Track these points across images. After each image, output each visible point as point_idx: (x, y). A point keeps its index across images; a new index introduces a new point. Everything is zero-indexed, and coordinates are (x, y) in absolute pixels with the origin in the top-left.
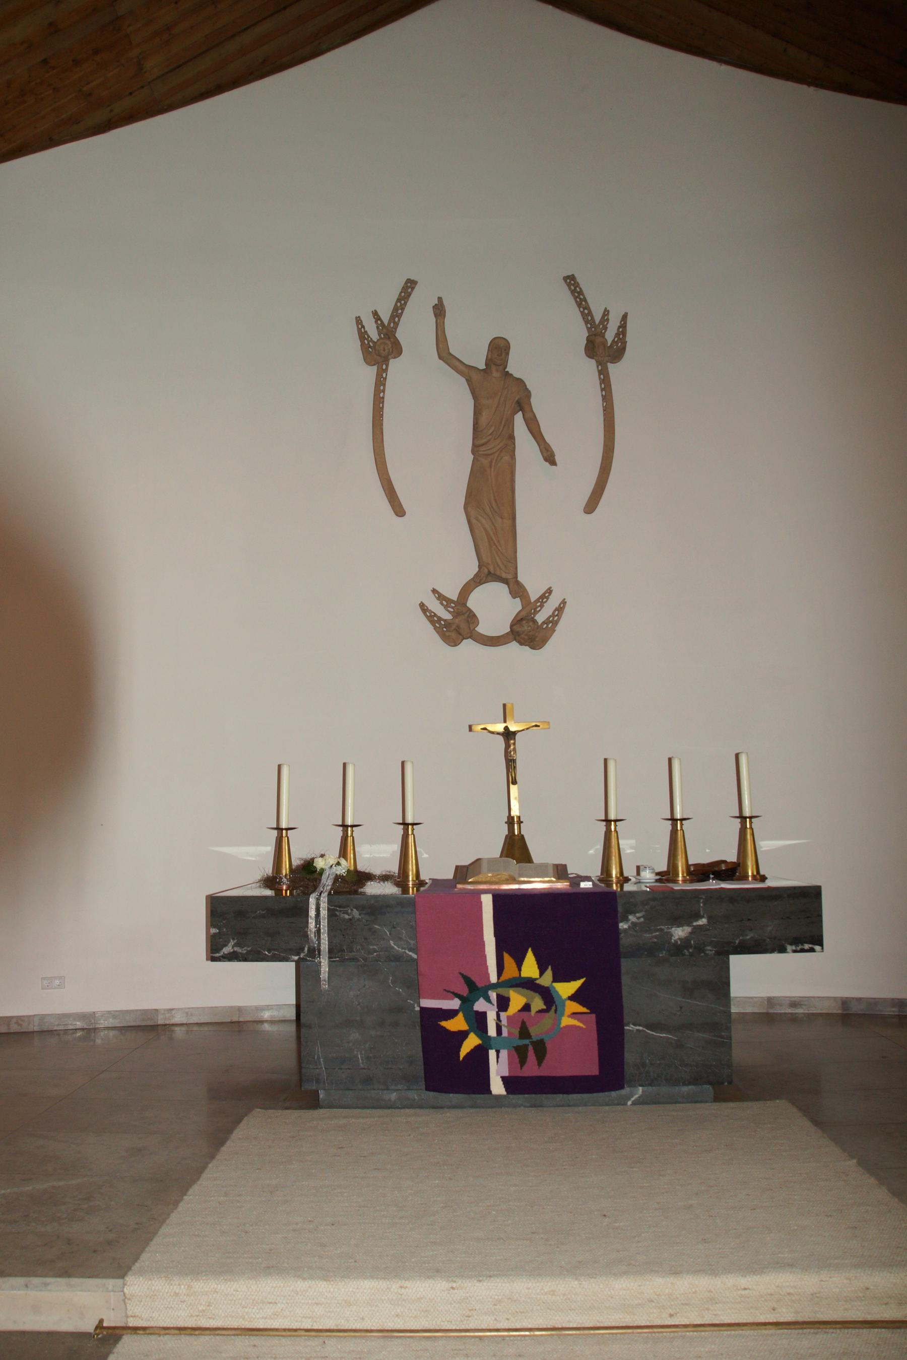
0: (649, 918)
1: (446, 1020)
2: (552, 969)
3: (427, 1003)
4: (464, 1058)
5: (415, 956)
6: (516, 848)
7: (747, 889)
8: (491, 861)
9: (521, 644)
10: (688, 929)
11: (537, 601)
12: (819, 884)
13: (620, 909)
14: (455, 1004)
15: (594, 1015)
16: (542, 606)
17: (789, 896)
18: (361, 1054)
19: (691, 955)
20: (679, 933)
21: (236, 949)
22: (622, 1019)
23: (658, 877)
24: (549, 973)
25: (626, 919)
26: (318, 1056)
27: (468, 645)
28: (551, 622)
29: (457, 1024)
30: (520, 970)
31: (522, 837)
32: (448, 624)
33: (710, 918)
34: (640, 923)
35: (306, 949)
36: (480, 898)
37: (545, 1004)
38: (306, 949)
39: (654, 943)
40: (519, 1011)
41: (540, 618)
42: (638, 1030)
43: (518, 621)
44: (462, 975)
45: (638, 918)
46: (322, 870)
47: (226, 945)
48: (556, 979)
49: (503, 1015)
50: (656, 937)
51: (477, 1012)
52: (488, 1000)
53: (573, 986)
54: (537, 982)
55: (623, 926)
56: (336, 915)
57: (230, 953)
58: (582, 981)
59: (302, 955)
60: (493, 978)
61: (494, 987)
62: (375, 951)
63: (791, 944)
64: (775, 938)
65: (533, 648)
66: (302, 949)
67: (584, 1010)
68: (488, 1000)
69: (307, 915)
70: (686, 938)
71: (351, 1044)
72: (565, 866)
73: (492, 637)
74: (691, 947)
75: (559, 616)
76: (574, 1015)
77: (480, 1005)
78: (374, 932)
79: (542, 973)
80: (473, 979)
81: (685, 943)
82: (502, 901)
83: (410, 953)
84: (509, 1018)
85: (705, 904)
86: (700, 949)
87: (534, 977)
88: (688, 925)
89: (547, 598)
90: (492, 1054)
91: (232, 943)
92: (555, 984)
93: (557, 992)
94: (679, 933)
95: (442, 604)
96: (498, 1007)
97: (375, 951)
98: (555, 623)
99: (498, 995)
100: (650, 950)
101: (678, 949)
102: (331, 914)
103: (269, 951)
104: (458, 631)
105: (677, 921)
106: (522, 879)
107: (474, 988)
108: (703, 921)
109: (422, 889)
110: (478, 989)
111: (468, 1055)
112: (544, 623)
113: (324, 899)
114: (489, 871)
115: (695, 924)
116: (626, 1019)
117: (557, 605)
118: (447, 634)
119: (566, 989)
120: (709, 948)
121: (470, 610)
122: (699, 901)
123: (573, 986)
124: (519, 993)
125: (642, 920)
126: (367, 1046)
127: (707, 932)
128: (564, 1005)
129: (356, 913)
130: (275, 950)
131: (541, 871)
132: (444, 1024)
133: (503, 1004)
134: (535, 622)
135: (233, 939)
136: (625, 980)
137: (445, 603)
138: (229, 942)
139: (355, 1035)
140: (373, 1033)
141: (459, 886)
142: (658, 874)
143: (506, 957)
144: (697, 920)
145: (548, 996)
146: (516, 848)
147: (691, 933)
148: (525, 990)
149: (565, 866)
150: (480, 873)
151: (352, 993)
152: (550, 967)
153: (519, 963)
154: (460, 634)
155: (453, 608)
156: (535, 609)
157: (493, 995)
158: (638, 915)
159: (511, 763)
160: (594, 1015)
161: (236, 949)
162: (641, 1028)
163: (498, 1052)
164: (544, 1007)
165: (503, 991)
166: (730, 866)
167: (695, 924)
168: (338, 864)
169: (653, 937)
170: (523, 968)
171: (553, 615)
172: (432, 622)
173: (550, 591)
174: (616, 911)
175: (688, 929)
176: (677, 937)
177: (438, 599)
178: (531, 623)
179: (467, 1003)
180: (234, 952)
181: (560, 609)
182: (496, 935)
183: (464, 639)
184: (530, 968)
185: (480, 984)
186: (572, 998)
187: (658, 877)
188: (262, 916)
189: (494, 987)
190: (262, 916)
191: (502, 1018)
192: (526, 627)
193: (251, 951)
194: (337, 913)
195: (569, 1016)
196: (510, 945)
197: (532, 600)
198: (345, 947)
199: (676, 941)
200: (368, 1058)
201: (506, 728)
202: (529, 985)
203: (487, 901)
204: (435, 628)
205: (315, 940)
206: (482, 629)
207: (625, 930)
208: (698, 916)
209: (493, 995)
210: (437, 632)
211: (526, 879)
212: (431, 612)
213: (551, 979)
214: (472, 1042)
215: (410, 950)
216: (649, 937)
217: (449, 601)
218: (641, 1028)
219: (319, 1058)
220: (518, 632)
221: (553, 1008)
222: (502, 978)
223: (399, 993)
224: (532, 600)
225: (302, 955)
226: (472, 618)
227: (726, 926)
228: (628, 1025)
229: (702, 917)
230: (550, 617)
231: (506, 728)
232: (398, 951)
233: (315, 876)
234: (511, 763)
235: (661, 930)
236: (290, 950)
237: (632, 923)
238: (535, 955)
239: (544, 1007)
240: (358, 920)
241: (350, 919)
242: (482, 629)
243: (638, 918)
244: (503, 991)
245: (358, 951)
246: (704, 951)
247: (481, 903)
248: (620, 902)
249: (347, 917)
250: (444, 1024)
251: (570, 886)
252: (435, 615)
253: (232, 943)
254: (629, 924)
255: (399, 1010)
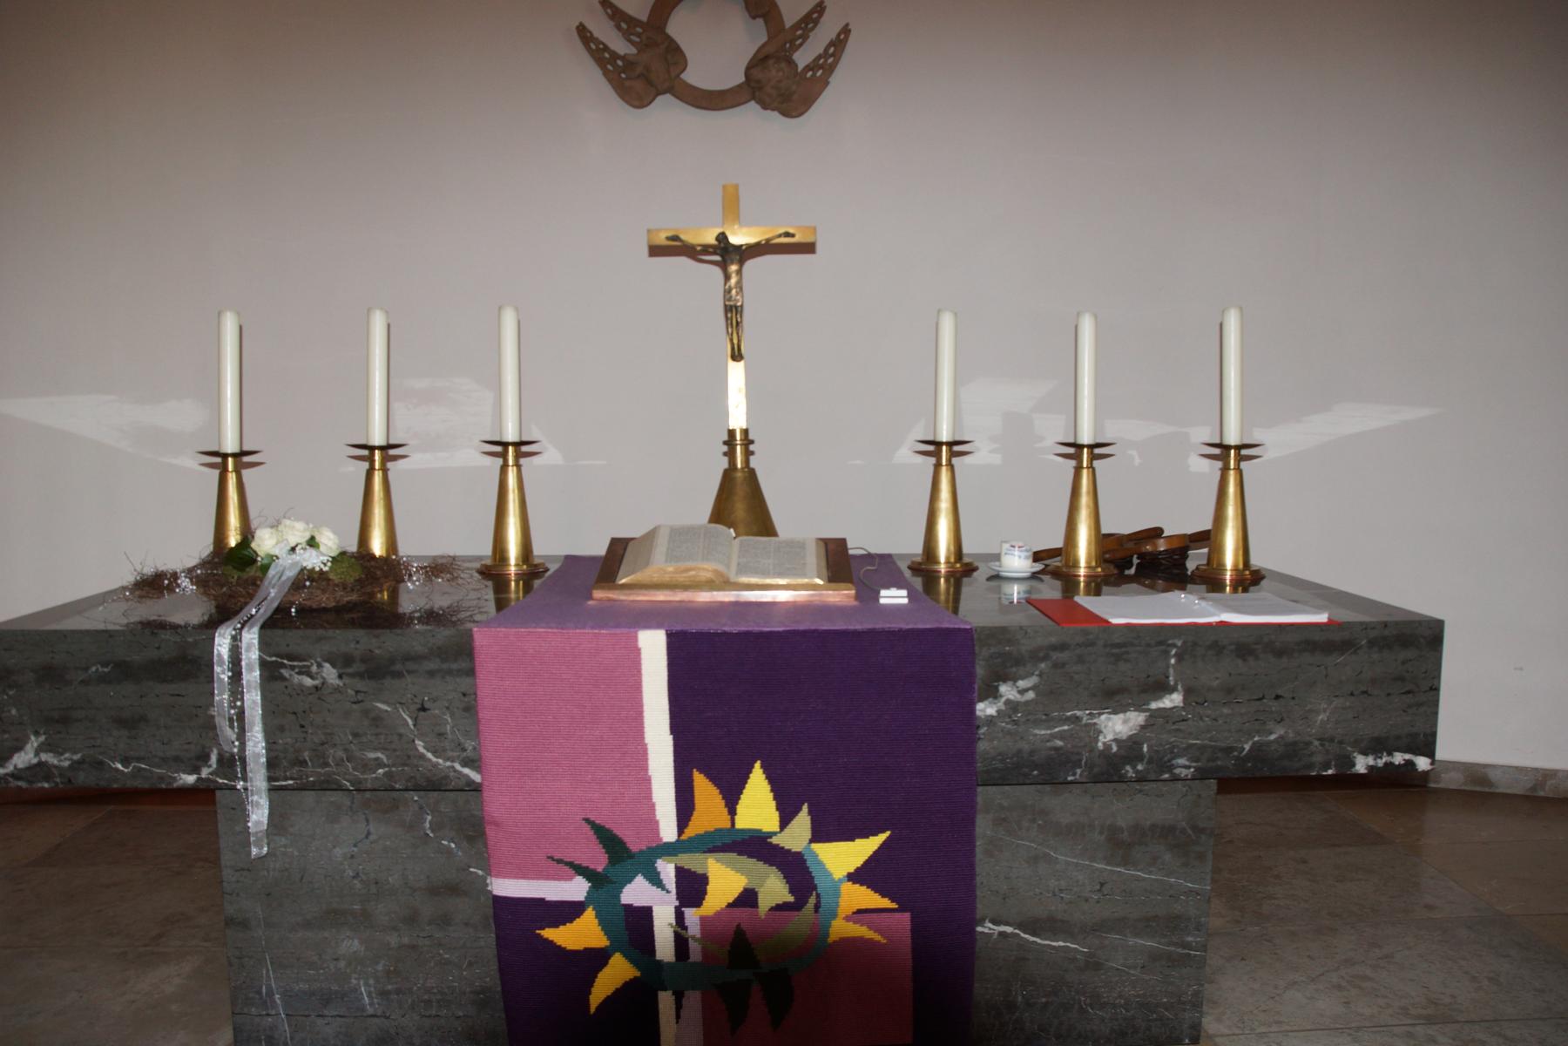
0: (1049, 693)
1: (556, 925)
2: (810, 813)
3: (507, 887)
4: (598, 1009)
5: (476, 777)
6: (741, 503)
7: (1280, 626)
8: (681, 534)
9: (765, 107)
10: (1136, 719)
11: (796, 26)
12: (1406, 592)
13: (980, 671)
14: (575, 889)
15: (907, 915)
16: (805, 37)
17: (1372, 643)
18: (366, 984)
19: (1141, 779)
20: (1117, 726)
21: (44, 757)
22: (974, 909)
23: (1039, 567)
24: (803, 821)
25: (992, 693)
26: (269, 988)
27: (666, 110)
28: (821, 67)
29: (583, 933)
30: (732, 812)
31: (751, 475)
32: (629, 63)
33: (1188, 693)
34: (1027, 703)
35: (214, 758)
36: (636, 639)
37: (791, 891)
38: (214, 758)
39: (1056, 749)
40: (730, 905)
41: (803, 58)
42: (1001, 934)
43: (758, 62)
44: (587, 820)
45: (1022, 692)
46: (272, 558)
47: (19, 749)
48: (819, 835)
49: (691, 915)
50: (1061, 736)
51: (629, 907)
52: (656, 880)
53: (862, 849)
54: (774, 840)
55: (985, 709)
56: (283, 679)
57: (31, 768)
58: (882, 837)
59: (205, 773)
60: (668, 832)
61: (668, 850)
62: (380, 764)
63: (1365, 753)
64: (1332, 740)
65: (786, 114)
66: (205, 758)
67: (886, 903)
68: (656, 880)
69: (210, 678)
70: (1130, 737)
71: (342, 964)
72: (843, 541)
73: (711, 93)
74: (1140, 758)
75: (837, 56)
76: (861, 914)
77: (636, 892)
78: (377, 720)
79: (785, 822)
80: (618, 832)
81: (1130, 748)
82: (694, 655)
83: (466, 771)
84: (703, 919)
85: (1179, 657)
86: (1161, 763)
87: (766, 829)
88: (1139, 709)
89: (816, 22)
90: (666, 1000)
91: (34, 742)
92: (816, 847)
93: (820, 864)
94: (1117, 726)
95: (619, 28)
96: (679, 896)
97: (380, 764)
98: (830, 69)
99: (680, 871)
100: (1049, 771)
101: (1111, 769)
102: (270, 672)
103: (126, 761)
104: (646, 77)
105: (1114, 698)
106: (745, 580)
107: (622, 855)
108: (1174, 700)
109: (537, 583)
110: (631, 855)
111: (608, 1001)
112: (808, 68)
113: (251, 637)
114: (670, 557)
115: (1154, 705)
116: (981, 909)
117: (833, 36)
118: (627, 83)
119: (841, 858)
120: (1182, 761)
121: (669, 37)
122: (1166, 653)
123: (862, 849)
124: (728, 864)
125: (1031, 695)
126: (380, 967)
127: (1182, 726)
128: (837, 894)
129: (330, 673)
130: (139, 760)
131: (789, 564)
132: (549, 933)
133: (691, 888)
134: (791, 63)
135: (37, 734)
136: (983, 826)
137: (624, 26)
138: (25, 741)
139: (351, 945)
140: (393, 940)
141: (598, 594)
142: (1037, 557)
143: (700, 782)
144: (1160, 698)
145: (796, 869)
146: (741, 503)
147: (1143, 727)
148: (744, 858)
149: (843, 541)
150: (647, 564)
151: (338, 852)
152: (805, 808)
153: (732, 796)
154: (650, 83)
155: (639, 35)
156: (792, 42)
157: (667, 869)
158: (1022, 684)
159: (559, 861)
160: (907, 915)
161: (44, 757)
162: (1009, 929)
163: (679, 997)
164: (791, 899)
165: (691, 861)
166: (1176, 545)
167: (1154, 705)
168: (312, 543)
169: (1054, 736)
170: (740, 808)
171: (825, 54)
172: (601, 62)
173: (820, 9)
174: (971, 675)
175: (1136, 719)
176: (1110, 737)
177: (612, 17)
178: (783, 65)
179: (604, 884)
180: (40, 764)
181: (839, 44)
182: (675, 729)
183: (659, 94)
184: (757, 806)
185: (635, 845)
186: (856, 877)
187: (1039, 567)
188: (102, 679)
189: (668, 850)
190: (102, 679)
191: (688, 922)
192: (774, 73)
193: (79, 762)
194: (285, 672)
195: (848, 919)
196: (708, 752)
197: (788, 24)
198: (306, 755)
199: (1107, 747)
200: (384, 994)
201: (722, 238)
202: (755, 846)
203: (653, 646)
204: (606, 73)
205: (231, 734)
206: (694, 76)
207: (990, 720)
208: (1163, 688)
209: (667, 869)
210: (610, 81)
211: (754, 580)
212: (597, 41)
213: (808, 835)
214: (617, 972)
215: (465, 765)
216: (1046, 736)
217: (632, 21)
218: (1009, 929)
219: (270, 994)
220: (758, 81)
221: (812, 900)
222: (690, 832)
223: (449, 851)
224: (788, 24)
225: (205, 773)
226: (674, 55)
227: (1225, 711)
228: (981, 922)
229: (1173, 690)
230: (820, 57)
231: (722, 238)
232: (436, 765)
233: (252, 572)
234: (559, 861)
235: (1078, 719)
236: (177, 759)
237: (1008, 702)
238: (771, 778)
239: (791, 899)
240: (337, 689)
241: (316, 688)
242: (694, 76)
243: (1022, 692)
244: (691, 861)
245: (339, 763)
246: (1170, 768)
247: (638, 651)
248: (982, 653)
249: (308, 682)
250: (549, 933)
251: (858, 597)
252: (606, 48)
253: (34, 742)
254: (1001, 704)
255: (453, 889)
